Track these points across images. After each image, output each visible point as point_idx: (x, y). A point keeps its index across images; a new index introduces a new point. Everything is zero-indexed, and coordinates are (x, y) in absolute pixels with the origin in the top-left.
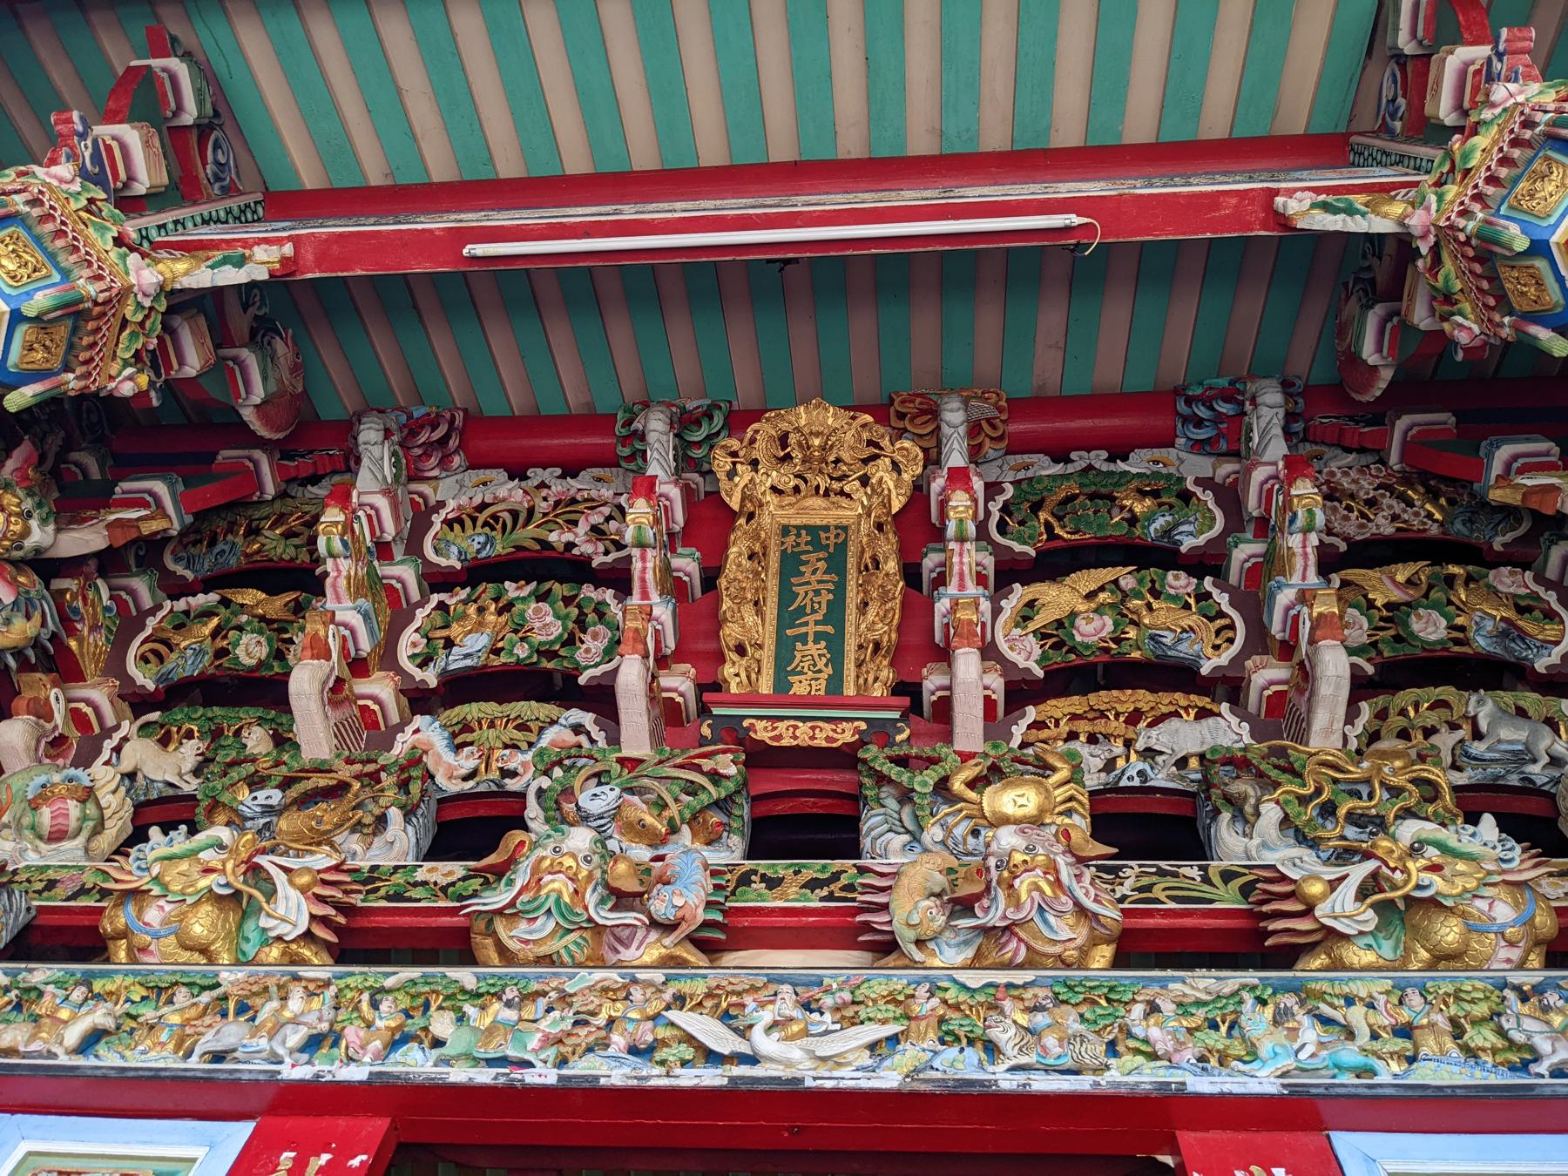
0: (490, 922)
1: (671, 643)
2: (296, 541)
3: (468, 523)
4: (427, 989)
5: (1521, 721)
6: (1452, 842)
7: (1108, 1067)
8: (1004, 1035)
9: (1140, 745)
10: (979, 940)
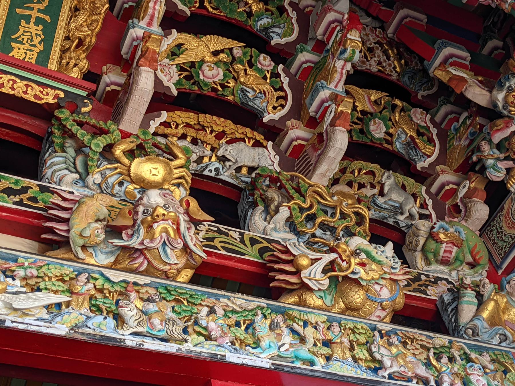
5: (402, 191)
6: (374, 254)
8: (130, 313)
9: (220, 153)
10: (118, 253)
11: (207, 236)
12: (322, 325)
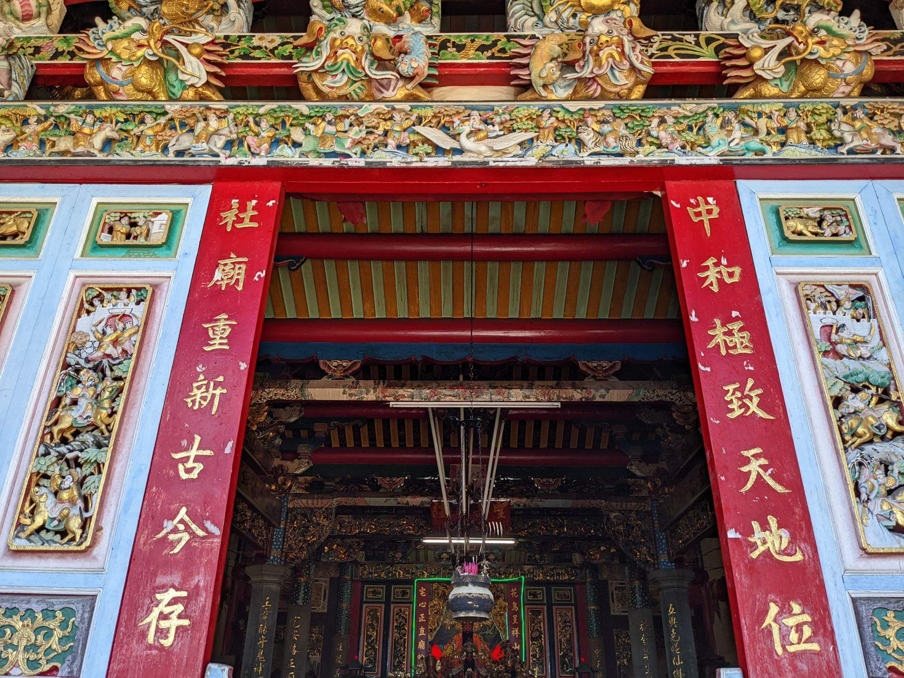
0: (310, 76)
4: (282, 114)
6: (835, 28)
7: (638, 153)
8: (587, 137)
10: (575, 84)
11: (661, 46)
12: (777, 113)
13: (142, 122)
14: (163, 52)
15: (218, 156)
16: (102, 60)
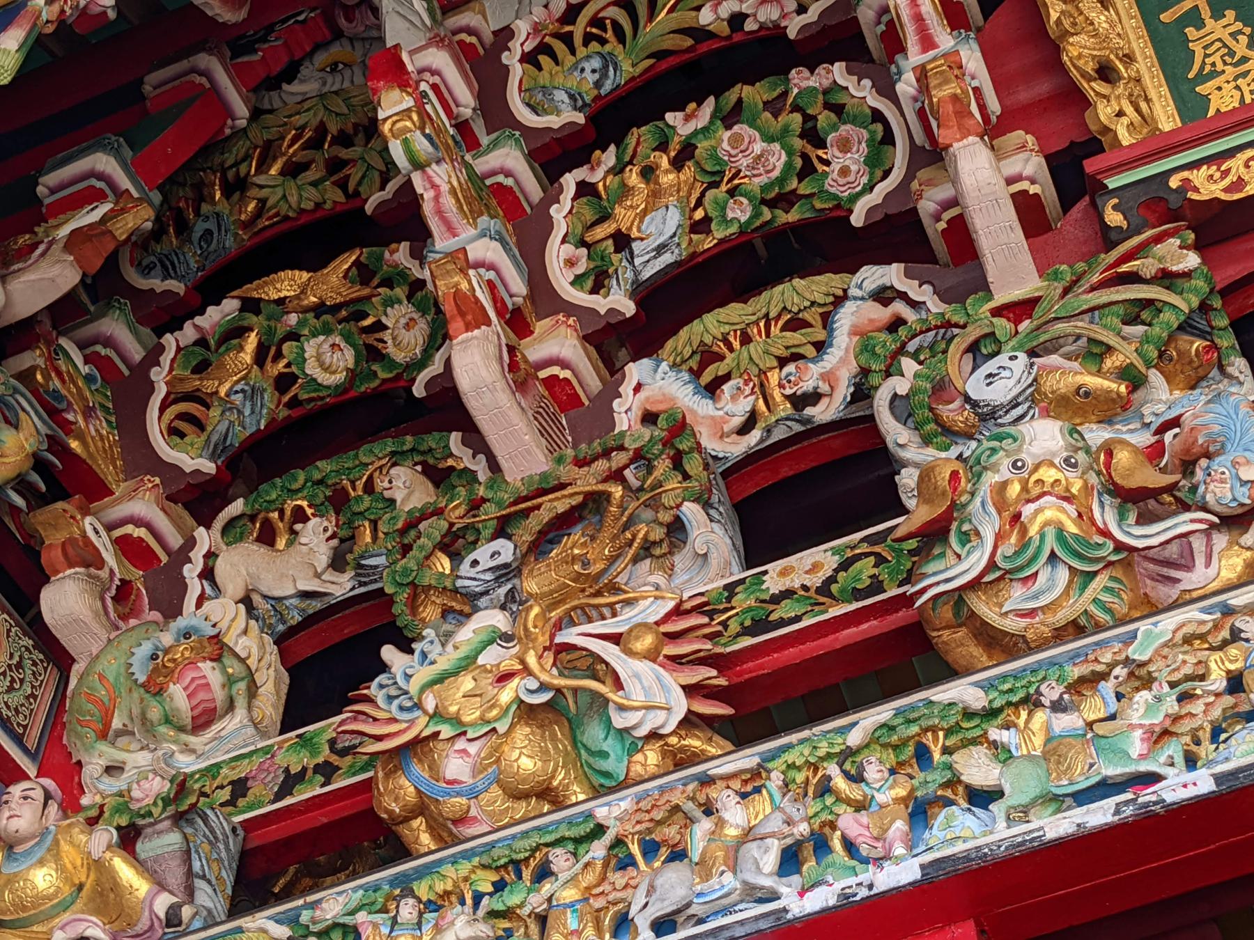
0: (960, 603)
1: (994, 106)
2: (312, 174)
3: (559, 47)
4: (914, 729)
13: (544, 873)
14: (561, 674)
15: (774, 896)
16: (417, 742)
